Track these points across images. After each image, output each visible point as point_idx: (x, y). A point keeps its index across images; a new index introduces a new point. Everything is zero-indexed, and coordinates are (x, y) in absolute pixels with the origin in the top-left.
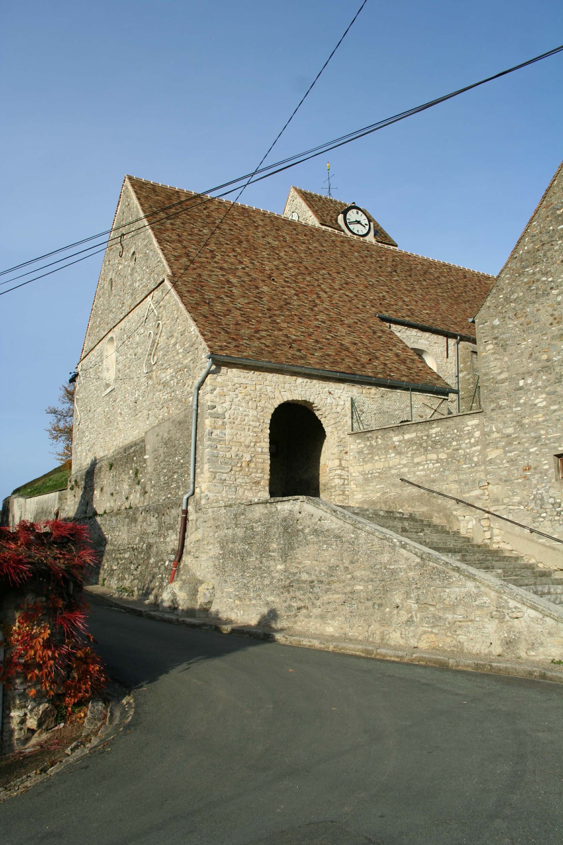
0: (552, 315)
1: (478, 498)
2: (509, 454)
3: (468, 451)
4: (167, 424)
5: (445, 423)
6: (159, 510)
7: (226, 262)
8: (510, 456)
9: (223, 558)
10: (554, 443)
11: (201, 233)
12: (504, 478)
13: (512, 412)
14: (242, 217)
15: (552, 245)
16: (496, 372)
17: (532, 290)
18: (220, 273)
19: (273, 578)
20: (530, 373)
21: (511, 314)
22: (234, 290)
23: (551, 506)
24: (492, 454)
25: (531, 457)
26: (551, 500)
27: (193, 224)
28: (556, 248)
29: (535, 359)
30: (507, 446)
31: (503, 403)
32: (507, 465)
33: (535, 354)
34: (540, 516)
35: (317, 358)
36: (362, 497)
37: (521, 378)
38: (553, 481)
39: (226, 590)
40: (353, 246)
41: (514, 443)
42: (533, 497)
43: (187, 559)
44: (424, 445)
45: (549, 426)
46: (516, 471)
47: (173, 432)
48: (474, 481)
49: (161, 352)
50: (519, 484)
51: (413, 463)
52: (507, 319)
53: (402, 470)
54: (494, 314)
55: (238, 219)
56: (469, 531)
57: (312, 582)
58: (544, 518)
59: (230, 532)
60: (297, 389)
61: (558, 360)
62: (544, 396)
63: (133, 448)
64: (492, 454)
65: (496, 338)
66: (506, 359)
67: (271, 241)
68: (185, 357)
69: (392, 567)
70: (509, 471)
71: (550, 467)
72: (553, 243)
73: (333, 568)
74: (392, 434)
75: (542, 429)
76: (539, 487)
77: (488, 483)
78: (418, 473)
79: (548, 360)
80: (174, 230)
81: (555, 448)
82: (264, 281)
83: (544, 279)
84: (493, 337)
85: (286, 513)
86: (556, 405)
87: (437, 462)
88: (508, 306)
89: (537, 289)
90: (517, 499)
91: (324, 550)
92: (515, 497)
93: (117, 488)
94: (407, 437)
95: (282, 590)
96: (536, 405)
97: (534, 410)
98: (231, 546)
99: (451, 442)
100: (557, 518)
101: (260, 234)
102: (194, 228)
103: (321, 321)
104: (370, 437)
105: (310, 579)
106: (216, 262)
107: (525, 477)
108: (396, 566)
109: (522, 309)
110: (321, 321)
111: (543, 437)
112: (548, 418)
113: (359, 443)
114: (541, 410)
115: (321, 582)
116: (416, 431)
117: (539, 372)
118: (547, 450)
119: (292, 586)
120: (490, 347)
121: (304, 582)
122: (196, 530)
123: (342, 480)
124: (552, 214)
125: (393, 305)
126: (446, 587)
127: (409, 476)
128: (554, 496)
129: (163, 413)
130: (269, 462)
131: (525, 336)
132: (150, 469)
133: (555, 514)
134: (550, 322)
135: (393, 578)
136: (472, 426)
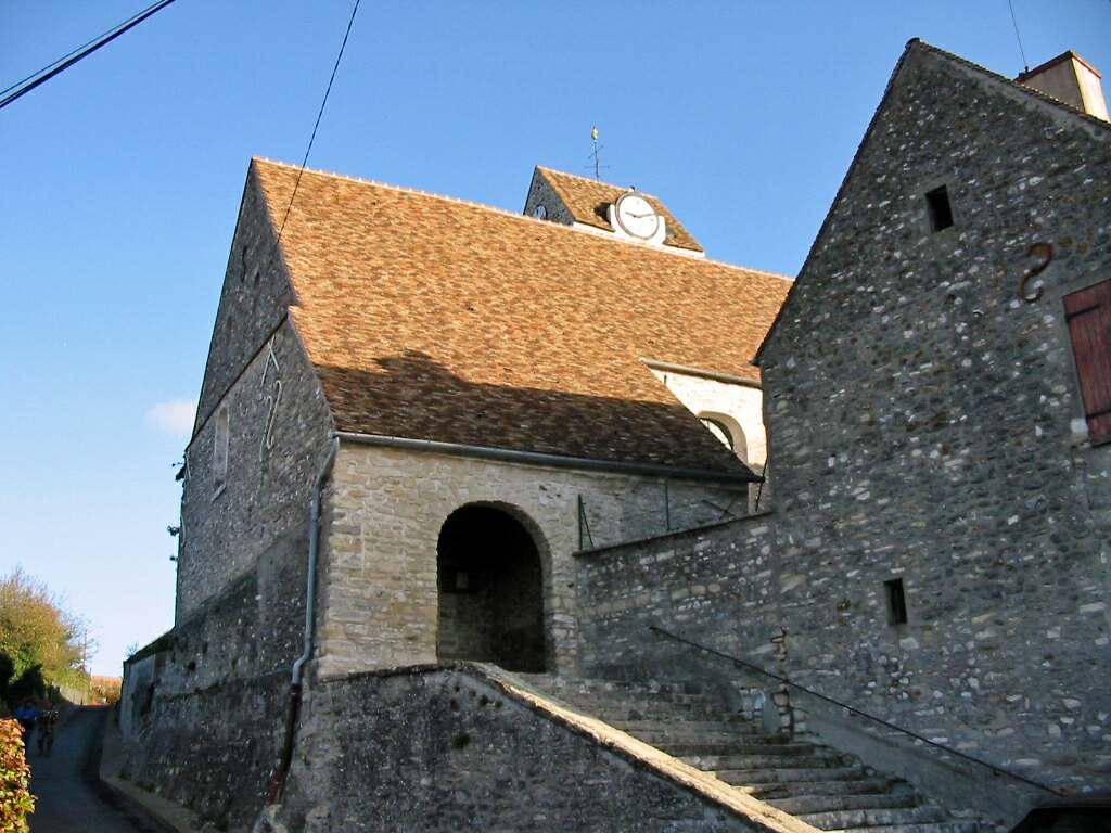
0: (875, 348)
1: (769, 658)
2: (815, 583)
3: (753, 578)
4: (283, 544)
5: (717, 532)
6: (266, 685)
7: (397, 284)
8: (816, 587)
9: (345, 765)
10: (883, 561)
11: (362, 241)
12: (807, 624)
13: (818, 512)
14: (435, 215)
15: (871, 233)
16: (794, 445)
17: (842, 308)
18: (383, 302)
19: (415, 799)
20: (844, 447)
21: (812, 350)
22: (402, 328)
23: (883, 670)
24: (790, 583)
25: (849, 586)
26: (883, 659)
27: (350, 228)
28: (878, 237)
29: (852, 422)
30: (810, 569)
31: (804, 496)
32: (812, 601)
33: (851, 412)
34: (866, 688)
35: (522, 433)
36: (596, 659)
37: (830, 454)
38: (885, 626)
39: (347, 819)
40: (618, 253)
41: (823, 563)
42: (853, 654)
43: (296, 766)
44: (687, 570)
45: (875, 534)
46: (826, 612)
47: (290, 557)
48: (762, 630)
49: (280, 429)
50: (832, 632)
51: (671, 601)
52: (806, 358)
53: (654, 613)
54: (788, 349)
55: (428, 218)
56: (756, 713)
57: (472, 807)
58: (871, 689)
59: (356, 722)
60: (488, 483)
61: (887, 423)
62: (866, 483)
63: (245, 584)
64: (790, 583)
65: (791, 390)
66: (807, 423)
67: (480, 251)
68: (307, 437)
69: (591, 782)
70: (815, 611)
71: (880, 604)
72: (873, 230)
73: (502, 784)
74: (638, 553)
75: (865, 538)
76: (863, 637)
77: (785, 633)
78: (679, 617)
79: (871, 423)
80: (318, 238)
81: (886, 570)
82: (456, 312)
83: (861, 289)
84: (786, 387)
85: (437, 690)
86: (885, 497)
87: (707, 599)
88: (808, 336)
89: (852, 305)
90: (829, 658)
91: (489, 753)
92: (826, 656)
93: (224, 648)
94: (661, 557)
95: (426, 821)
96: (854, 498)
97: (852, 507)
98: (356, 744)
99: (726, 565)
100: (892, 690)
101: (463, 240)
102: (351, 233)
103: (544, 374)
104: (607, 559)
105: (468, 802)
106: (379, 286)
107: (840, 621)
108: (597, 781)
109: (829, 341)
110: (544, 374)
111: (867, 551)
112: (874, 519)
113: (590, 570)
114: (861, 506)
115: (484, 807)
116: (674, 548)
117: (858, 442)
118: (873, 574)
119: (442, 814)
120: (782, 404)
121: (461, 807)
122: (310, 717)
123: (564, 631)
124: (870, 183)
125: (674, 344)
126: (673, 819)
127: (664, 622)
128: (888, 651)
129: (279, 528)
130: (436, 603)
131: (835, 383)
132: (262, 618)
133: (889, 682)
134: (872, 359)
135: (591, 802)
136: (758, 536)
